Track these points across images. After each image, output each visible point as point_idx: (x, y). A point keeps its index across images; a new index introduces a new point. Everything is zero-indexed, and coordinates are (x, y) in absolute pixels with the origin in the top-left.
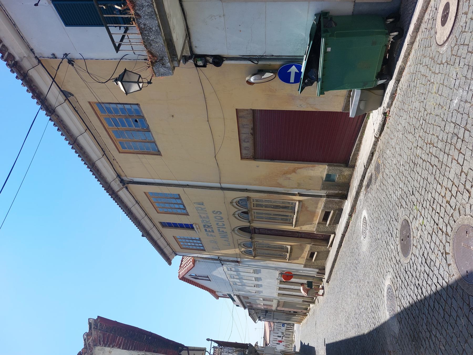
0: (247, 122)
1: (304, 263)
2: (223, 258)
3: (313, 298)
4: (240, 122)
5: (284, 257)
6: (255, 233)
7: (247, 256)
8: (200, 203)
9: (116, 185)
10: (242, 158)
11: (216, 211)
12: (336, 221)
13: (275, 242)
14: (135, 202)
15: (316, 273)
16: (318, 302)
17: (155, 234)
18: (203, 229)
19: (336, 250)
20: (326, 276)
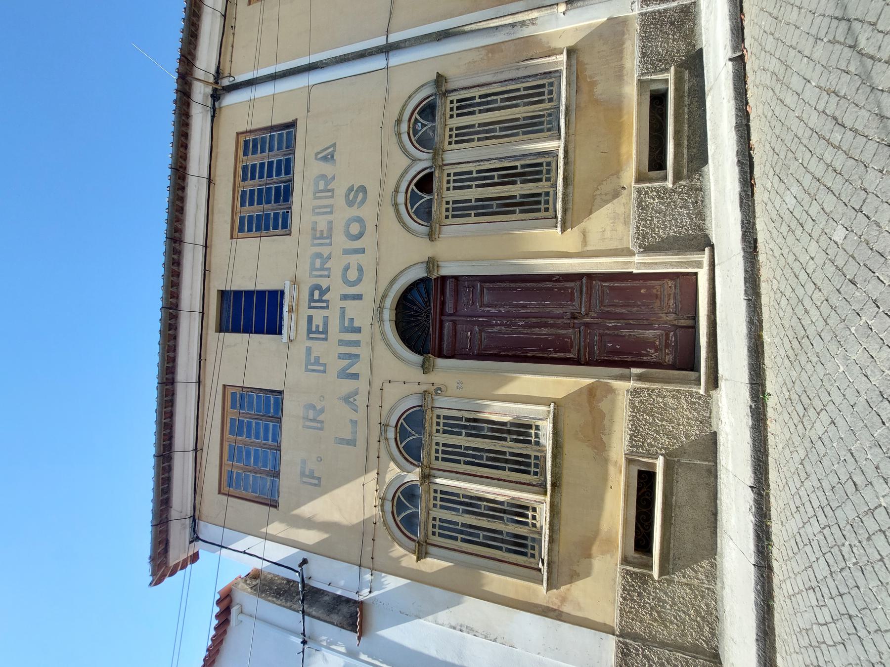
14: (206, 175)
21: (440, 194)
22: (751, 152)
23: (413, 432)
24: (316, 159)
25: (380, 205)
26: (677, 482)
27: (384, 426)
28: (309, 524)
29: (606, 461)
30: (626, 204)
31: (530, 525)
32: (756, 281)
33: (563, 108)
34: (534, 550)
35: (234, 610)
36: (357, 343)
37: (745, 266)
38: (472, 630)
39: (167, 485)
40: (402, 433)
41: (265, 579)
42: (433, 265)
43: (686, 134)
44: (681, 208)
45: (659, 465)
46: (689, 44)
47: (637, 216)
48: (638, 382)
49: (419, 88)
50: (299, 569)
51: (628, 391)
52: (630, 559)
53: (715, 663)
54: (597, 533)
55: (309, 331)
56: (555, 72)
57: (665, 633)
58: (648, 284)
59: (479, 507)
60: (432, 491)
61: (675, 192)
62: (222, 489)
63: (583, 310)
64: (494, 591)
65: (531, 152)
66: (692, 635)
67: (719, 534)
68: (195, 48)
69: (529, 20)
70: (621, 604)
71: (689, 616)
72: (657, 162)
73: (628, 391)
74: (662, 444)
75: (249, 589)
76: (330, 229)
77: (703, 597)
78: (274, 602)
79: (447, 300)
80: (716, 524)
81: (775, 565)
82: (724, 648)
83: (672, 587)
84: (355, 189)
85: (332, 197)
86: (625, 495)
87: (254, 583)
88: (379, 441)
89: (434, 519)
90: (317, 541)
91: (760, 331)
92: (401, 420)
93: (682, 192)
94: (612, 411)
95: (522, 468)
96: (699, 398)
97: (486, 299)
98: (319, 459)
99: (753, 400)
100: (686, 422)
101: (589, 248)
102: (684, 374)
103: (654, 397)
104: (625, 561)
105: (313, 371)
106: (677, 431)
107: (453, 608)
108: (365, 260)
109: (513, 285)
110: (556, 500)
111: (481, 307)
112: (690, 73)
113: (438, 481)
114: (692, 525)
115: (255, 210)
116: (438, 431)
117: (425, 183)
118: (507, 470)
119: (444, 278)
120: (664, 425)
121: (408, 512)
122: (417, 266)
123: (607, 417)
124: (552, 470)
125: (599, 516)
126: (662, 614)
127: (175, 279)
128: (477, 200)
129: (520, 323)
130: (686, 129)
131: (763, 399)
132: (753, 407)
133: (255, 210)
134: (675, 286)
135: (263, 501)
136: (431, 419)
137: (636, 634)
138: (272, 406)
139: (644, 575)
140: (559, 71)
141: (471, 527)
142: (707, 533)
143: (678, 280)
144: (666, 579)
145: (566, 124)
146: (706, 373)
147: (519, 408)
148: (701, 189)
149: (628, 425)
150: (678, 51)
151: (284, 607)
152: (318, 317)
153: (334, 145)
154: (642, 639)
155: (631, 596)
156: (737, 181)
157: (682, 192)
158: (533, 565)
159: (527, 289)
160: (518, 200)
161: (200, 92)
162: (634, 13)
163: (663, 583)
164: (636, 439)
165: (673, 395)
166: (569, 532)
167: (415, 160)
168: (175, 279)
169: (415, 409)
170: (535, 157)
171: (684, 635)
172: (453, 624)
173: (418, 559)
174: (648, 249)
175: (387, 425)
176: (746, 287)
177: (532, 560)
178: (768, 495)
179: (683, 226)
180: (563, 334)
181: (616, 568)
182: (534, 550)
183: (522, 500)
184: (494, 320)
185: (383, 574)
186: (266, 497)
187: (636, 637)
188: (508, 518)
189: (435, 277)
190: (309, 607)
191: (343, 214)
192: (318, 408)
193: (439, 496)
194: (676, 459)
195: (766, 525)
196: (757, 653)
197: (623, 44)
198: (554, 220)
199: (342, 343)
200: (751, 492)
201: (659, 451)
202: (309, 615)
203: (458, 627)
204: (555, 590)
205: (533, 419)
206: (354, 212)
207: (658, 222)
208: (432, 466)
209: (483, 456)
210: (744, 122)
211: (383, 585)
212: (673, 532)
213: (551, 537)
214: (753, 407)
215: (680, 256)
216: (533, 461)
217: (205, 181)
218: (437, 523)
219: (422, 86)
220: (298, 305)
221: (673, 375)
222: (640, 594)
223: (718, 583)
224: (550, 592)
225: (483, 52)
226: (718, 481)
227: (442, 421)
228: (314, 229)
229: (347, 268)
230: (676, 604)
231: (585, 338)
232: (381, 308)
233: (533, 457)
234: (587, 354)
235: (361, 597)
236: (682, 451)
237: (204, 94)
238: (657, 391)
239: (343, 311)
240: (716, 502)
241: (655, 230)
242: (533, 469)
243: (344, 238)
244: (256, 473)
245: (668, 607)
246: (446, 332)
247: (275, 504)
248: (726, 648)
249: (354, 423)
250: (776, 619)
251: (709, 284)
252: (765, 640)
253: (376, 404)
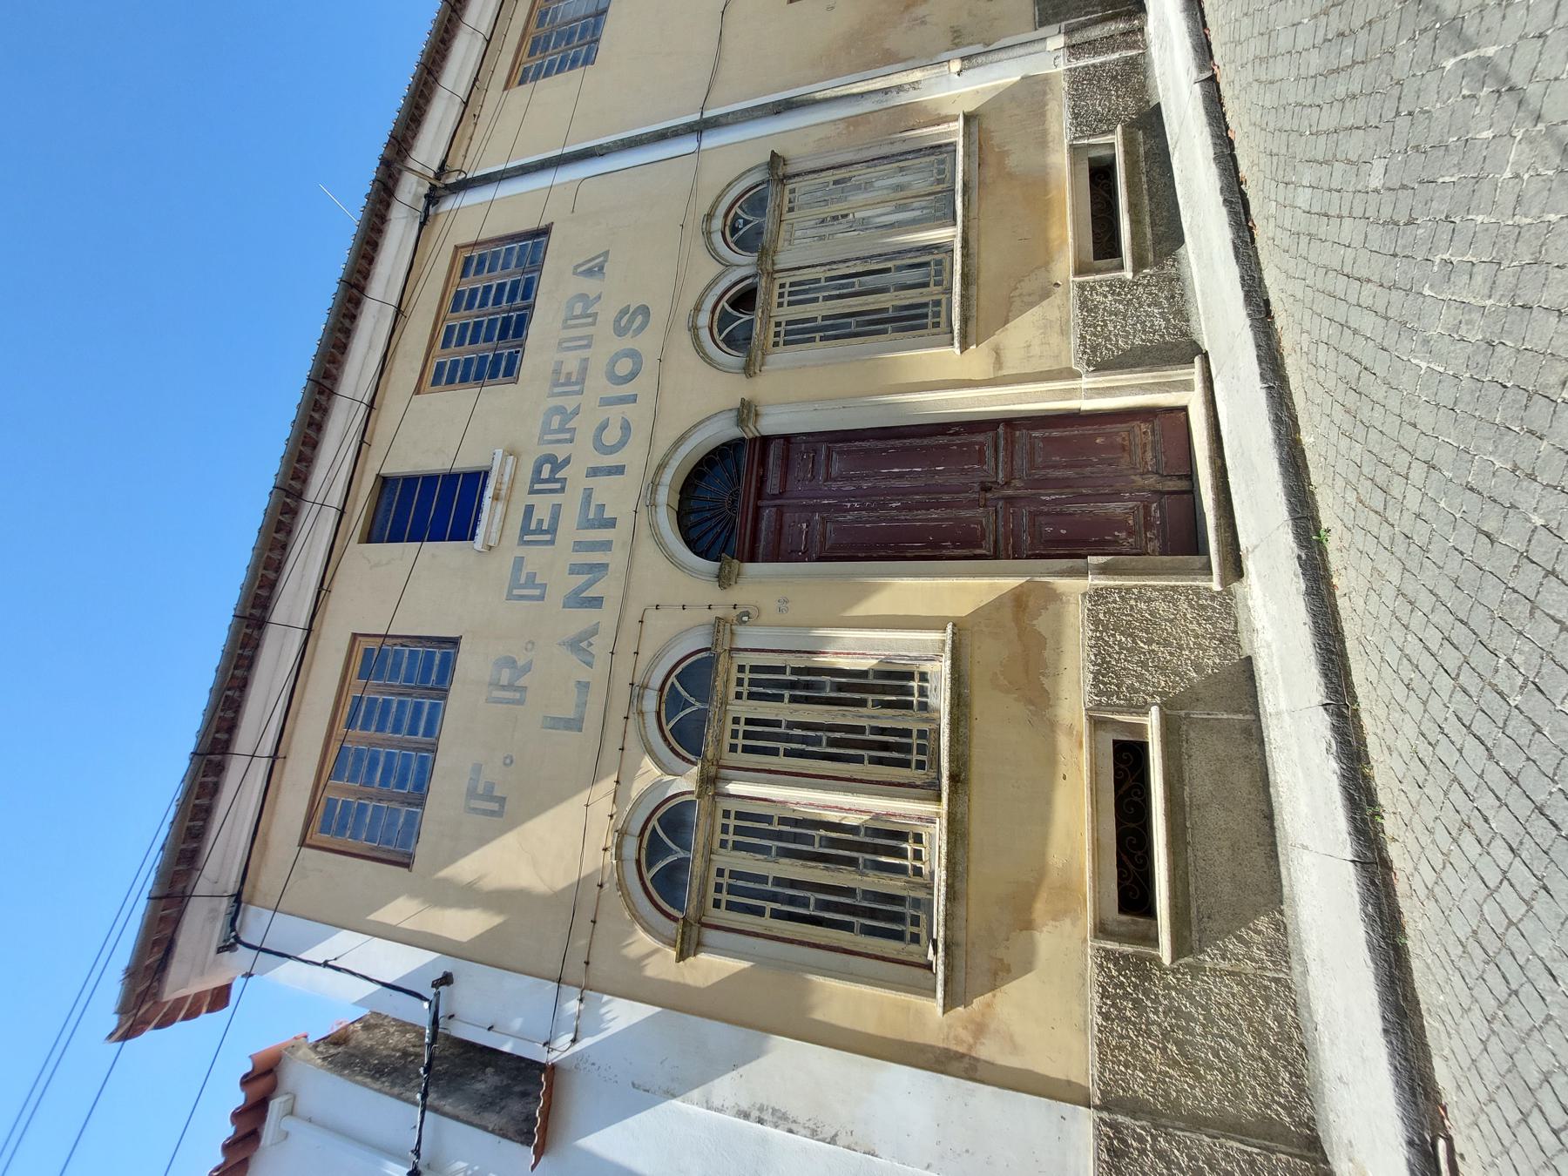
14: (394, 301)
22: (1243, 186)
23: (692, 700)
24: (575, 273)
25: (668, 331)
26: (1190, 756)
27: (638, 690)
28: (469, 896)
29: (1052, 725)
30: (1063, 307)
31: (910, 872)
32: (1276, 359)
33: (959, 186)
34: (918, 926)
35: (276, 1106)
36: (606, 546)
37: (1256, 339)
38: (784, 1117)
39: (201, 823)
40: (671, 701)
41: (355, 1047)
42: (749, 412)
43: (1148, 208)
44: (1149, 306)
45: (1152, 723)
46: (1141, 100)
47: (1080, 321)
48: (1102, 576)
49: (744, 173)
50: (429, 993)
51: (1084, 595)
52: (1112, 927)
53: (1314, 1162)
54: (1041, 871)
55: (525, 530)
56: (947, 145)
57: (1198, 1092)
58: (1108, 430)
59: (809, 840)
60: (720, 813)
61: (1138, 286)
62: (308, 836)
63: (1001, 476)
64: (833, 1022)
65: (912, 245)
66: (1255, 1095)
67: (1281, 858)
68: (414, 137)
69: (909, 84)
70: (1100, 1031)
71: (1244, 1047)
72: (1105, 244)
73: (1084, 595)
74: (1154, 686)
75: (319, 1061)
76: (584, 370)
77: (1267, 1000)
78: (364, 1085)
79: (770, 474)
80: (1275, 836)
81: (1393, 851)
82: (1327, 1120)
83: (1203, 981)
84: (631, 311)
85: (593, 324)
86: (1091, 790)
87: (332, 1051)
88: (627, 718)
89: (720, 873)
90: (479, 931)
91: (1295, 434)
92: (673, 679)
93: (1148, 284)
94: (1058, 634)
95: (895, 755)
96: (1213, 598)
97: (835, 469)
98: (508, 761)
99: (1301, 546)
100: (1194, 643)
101: (1005, 372)
102: (1181, 560)
103: (1133, 602)
104: (1102, 930)
105: (522, 597)
106: (1179, 660)
107: (747, 1067)
108: (638, 414)
109: (881, 444)
110: (960, 810)
111: (826, 480)
112: (1145, 134)
113: (733, 788)
114: (1228, 843)
115: (467, 352)
116: (739, 696)
117: (745, 299)
118: (866, 762)
119: (765, 441)
120: (1153, 651)
121: (670, 859)
122: (721, 416)
123: (1050, 643)
124: (950, 747)
125: (1044, 838)
126: (1188, 1048)
127: (307, 450)
128: (825, 318)
129: (894, 505)
130: (1147, 202)
131: (1319, 542)
132: (1304, 557)
133: (467, 352)
134: (1153, 431)
135: (384, 856)
136: (728, 672)
137: (1136, 1099)
138: (435, 669)
139: (1142, 959)
140: (954, 144)
141: (793, 884)
142: (1258, 855)
143: (1157, 422)
144: (1188, 966)
145: (964, 205)
146: (1219, 551)
147: (890, 640)
148: (1178, 279)
149: (1088, 655)
150: (1125, 109)
151: (386, 1093)
152: (543, 507)
153: (606, 253)
154: (1150, 1113)
155: (1120, 1010)
156: (1227, 226)
157: (1148, 284)
158: (915, 959)
159: (904, 449)
160: (891, 314)
161: (411, 189)
162: (1058, 69)
163: (1183, 974)
164: (1106, 680)
165: (1166, 596)
166: (984, 877)
167: (728, 266)
168: (307, 450)
169: (699, 656)
170: (918, 253)
171: (1239, 1095)
172: (745, 1106)
173: (682, 956)
174: (1101, 367)
175: (644, 687)
176: (1262, 369)
177: (913, 947)
178: (1356, 713)
179: (1155, 331)
180: (967, 518)
181: (1086, 948)
182: (918, 926)
183: (893, 819)
184: (849, 501)
185: (606, 998)
186: (392, 848)
187: (1135, 1108)
188: (865, 860)
189: (751, 435)
190: (438, 1098)
191: (607, 345)
192: (521, 663)
193: (732, 822)
194: (1182, 713)
195: (1363, 774)
196: (1391, 1064)
197: (1045, 104)
198: (949, 335)
199: (580, 546)
200: (1324, 713)
201: (1149, 699)
202: (436, 1110)
203: (755, 1114)
204: (960, 1009)
205: (916, 659)
206: (627, 343)
207: (1115, 327)
208: (722, 762)
209: (821, 737)
210: (1227, 152)
211: (602, 1022)
212: (1191, 860)
213: (950, 888)
214: (1304, 557)
215: (1154, 374)
216: (915, 741)
217: (391, 311)
218: (725, 880)
219: (749, 170)
220: (511, 488)
221: (1162, 562)
222: (1137, 1003)
223: (1293, 965)
224: (952, 1013)
225: (842, 126)
226: (1267, 749)
227: (747, 676)
228: (557, 372)
229: (603, 427)
230: (1213, 1022)
231: (1006, 522)
232: (654, 486)
233: (915, 734)
234: (1010, 548)
235: (555, 1054)
236: (1193, 697)
237: (415, 195)
238: (1135, 591)
239: (588, 494)
240: (1268, 792)
241: (1110, 340)
242: (915, 757)
243: (604, 381)
244: (380, 800)
245: (1198, 1029)
246: (764, 525)
247: (406, 861)
248: (1332, 1117)
249: (584, 687)
250: (1416, 975)
251: (1207, 409)
252: (1403, 1030)
253: (627, 646)
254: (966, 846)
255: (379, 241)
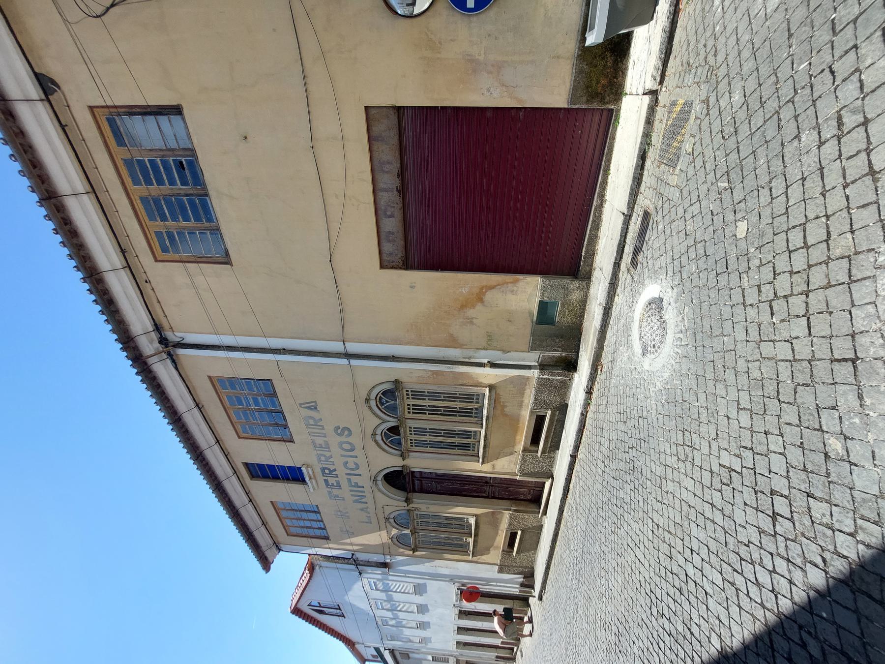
0: (387, 128)
1: (498, 563)
2: (362, 557)
3: (513, 649)
4: (375, 155)
5: (462, 549)
6: (414, 491)
7: (401, 550)
8: (311, 404)
9: (148, 345)
10: (382, 267)
11: (341, 428)
12: (555, 444)
13: (451, 509)
14: (192, 405)
15: (518, 586)
16: (522, 656)
17: (233, 487)
18: (321, 479)
19: (559, 503)
20: (536, 593)
21: (406, 437)
30: (517, 458)
217: (196, 411)
242: (475, 401)
254: (479, 529)
255: (159, 381)
